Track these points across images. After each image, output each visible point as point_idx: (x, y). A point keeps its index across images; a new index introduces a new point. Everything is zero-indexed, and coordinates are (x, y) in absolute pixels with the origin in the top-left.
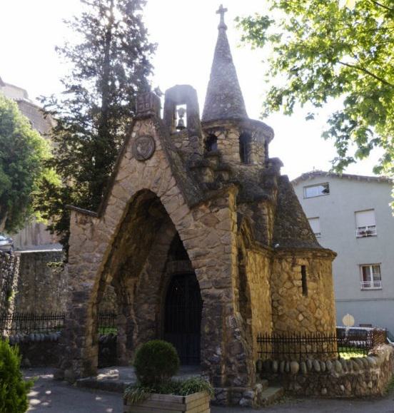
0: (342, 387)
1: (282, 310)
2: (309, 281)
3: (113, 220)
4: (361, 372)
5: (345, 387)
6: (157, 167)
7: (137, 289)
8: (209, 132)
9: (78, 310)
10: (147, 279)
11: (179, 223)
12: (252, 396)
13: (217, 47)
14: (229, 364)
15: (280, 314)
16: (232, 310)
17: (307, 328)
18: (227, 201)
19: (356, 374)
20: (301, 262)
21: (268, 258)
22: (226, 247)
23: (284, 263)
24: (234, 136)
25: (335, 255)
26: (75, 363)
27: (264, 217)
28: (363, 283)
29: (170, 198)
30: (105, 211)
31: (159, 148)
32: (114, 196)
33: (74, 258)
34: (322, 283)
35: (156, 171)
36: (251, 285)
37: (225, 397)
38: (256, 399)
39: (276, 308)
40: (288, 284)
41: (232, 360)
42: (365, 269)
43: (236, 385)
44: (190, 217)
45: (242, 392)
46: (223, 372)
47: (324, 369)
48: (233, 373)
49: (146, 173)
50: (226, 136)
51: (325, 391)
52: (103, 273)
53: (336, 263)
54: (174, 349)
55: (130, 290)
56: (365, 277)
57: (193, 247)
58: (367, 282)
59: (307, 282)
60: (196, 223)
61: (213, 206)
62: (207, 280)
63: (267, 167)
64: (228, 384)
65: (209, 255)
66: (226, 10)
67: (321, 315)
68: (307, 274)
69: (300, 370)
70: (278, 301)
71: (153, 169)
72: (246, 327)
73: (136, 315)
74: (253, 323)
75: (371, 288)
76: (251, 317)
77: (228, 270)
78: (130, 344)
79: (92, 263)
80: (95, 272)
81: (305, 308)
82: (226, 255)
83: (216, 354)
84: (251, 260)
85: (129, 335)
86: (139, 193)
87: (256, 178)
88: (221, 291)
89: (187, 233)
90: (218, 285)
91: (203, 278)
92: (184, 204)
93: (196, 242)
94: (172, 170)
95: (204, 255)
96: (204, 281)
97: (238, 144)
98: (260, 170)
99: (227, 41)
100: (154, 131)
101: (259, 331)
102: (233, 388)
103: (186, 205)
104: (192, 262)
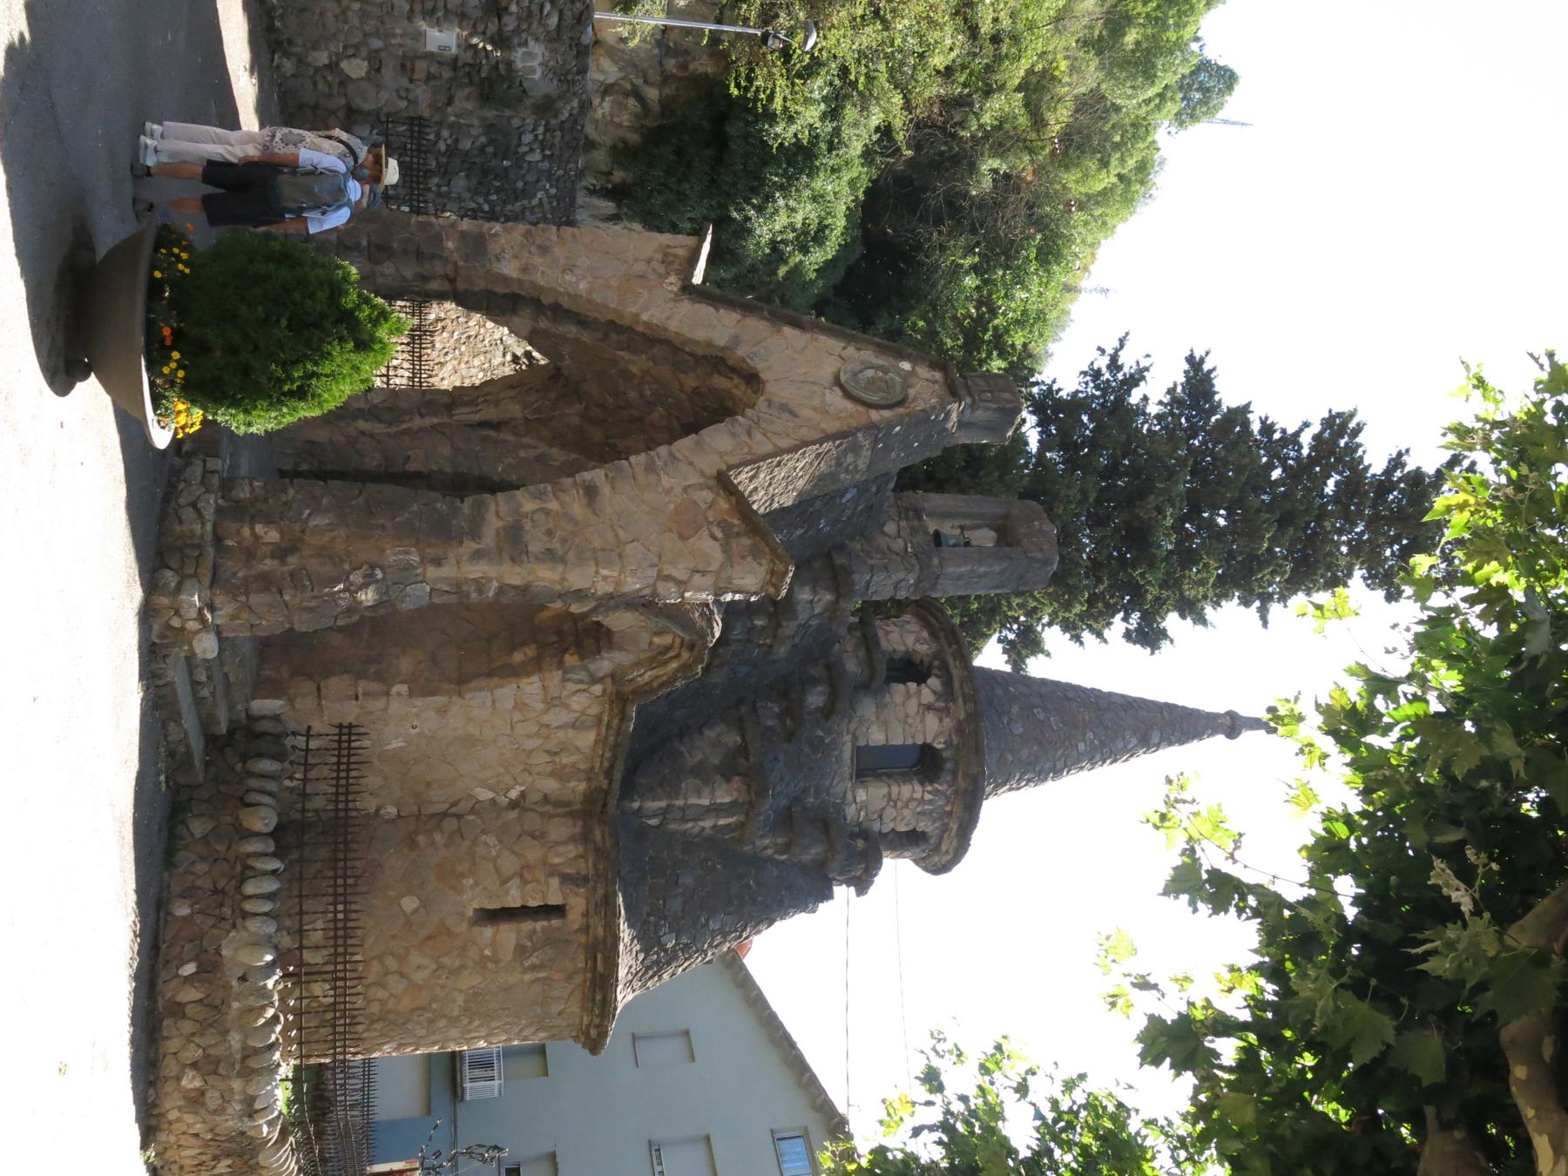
0: (189, 969)
1: (433, 844)
4: (235, 1040)
5: (188, 979)
6: (823, 410)
7: (492, 433)
10: (522, 454)
15: (421, 839)
20: (577, 905)
23: (572, 850)
24: (932, 730)
31: (875, 415)
34: (514, 978)
35: (814, 409)
39: (438, 827)
40: (509, 864)
47: (249, 906)
50: (929, 707)
60: (678, 490)
63: (853, 836)
68: (540, 925)
70: (459, 831)
71: (816, 402)
73: (421, 429)
76: (411, 694)
77: (550, 556)
84: (579, 702)
87: (817, 793)
98: (840, 809)
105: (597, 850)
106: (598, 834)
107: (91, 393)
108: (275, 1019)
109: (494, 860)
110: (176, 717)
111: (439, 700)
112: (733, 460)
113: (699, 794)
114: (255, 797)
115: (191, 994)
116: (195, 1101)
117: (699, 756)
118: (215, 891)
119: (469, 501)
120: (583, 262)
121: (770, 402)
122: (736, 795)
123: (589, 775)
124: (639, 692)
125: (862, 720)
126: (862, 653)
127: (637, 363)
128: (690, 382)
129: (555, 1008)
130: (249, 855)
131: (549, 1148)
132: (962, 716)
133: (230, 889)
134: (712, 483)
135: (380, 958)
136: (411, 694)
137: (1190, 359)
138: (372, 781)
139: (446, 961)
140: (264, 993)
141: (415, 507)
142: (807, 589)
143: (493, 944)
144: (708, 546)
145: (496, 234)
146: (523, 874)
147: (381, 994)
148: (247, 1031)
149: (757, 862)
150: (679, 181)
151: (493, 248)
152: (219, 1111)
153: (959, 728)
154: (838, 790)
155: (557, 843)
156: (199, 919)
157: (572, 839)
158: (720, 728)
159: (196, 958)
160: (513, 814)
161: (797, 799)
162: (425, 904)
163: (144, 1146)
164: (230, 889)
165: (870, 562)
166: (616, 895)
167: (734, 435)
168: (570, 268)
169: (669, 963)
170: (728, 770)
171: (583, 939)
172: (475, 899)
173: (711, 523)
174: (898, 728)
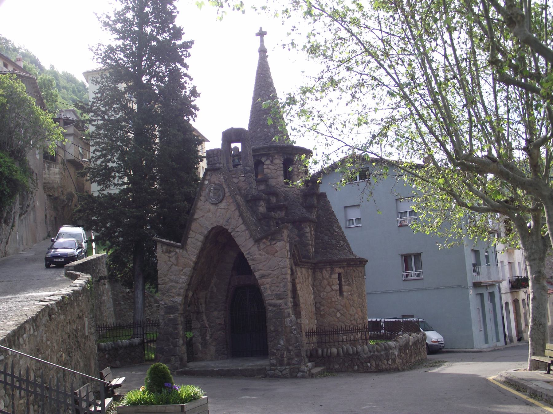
0: (369, 364)
1: (323, 310)
2: (344, 285)
3: (193, 250)
4: (383, 353)
8: (257, 158)
9: (171, 320)
11: (247, 252)
12: (306, 371)
13: (258, 71)
14: (289, 351)
16: (289, 314)
17: (343, 322)
18: (282, 236)
19: (379, 354)
20: (338, 270)
21: (311, 269)
22: (283, 270)
24: (279, 161)
25: (367, 261)
26: (173, 358)
27: (307, 234)
28: (404, 273)
29: (239, 233)
30: (186, 243)
31: (228, 194)
32: (193, 231)
33: (163, 280)
34: (355, 286)
35: (227, 212)
36: (300, 293)
37: (288, 372)
38: (308, 372)
39: (319, 308)
40: (328, 288)
41: (291, 348)
42: (406, 258)
43: (294, 364)
44: (255, 248)
45: (298, 369)
46: (285, 356)
48: (291, 357)
49: (218, 214)
50: (272, 162)
51: (356, 367)
52: (187, 290)
53: (367, 266)
56: (407, 267)
57: (259, 270)
58: (410, 272)
60: (260, 252)
61: (272, 240)
62: (270, 293)
64: (289, 364)
65: (271, 276)
66: (265, 33)
67: (355, 312)
69: (338, 353)
70: (320, 303)
72: (299, 325)
73: (208, 321)
74: (303, 322)
75: (413, 278)
78: (205, 344)
79: (178, 283)
80: (182, 291)
81: (342, 307)
82: (283, 276)
83: (280, 345)
84: (299, 273)
85: (203, 336)
86: (213, 229)
87: (298, 198)
88: (281, 301)
89: (253, 260)
90: (279, 297)
92: (250, 238)
93: (260, 266)
94: (239, 212)
95: (268, 276)
96: (269, 294)
97: (282, 169)
98: (302, 191)
99: (271, 84)
100: (223, 180)
101: (307, 327)
102: (292, 366)
103: (251, 239)
104: (259, 281)
109: (327, 293)
130: (343, 353)
135: (351, 321)
147: (359, 320)
149: (318, 217)
159: (366, 363)
161: (302, 205)
171: (346, 268)
173: (271, 244)
174: (278, 173)
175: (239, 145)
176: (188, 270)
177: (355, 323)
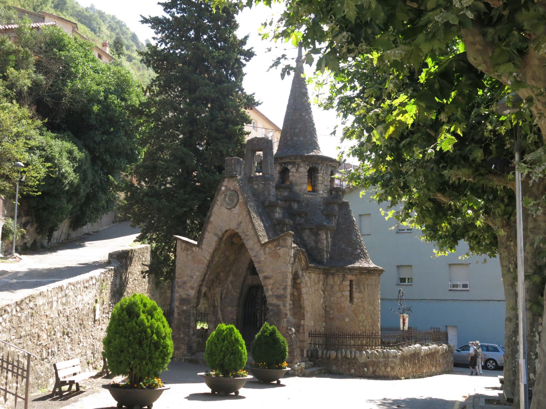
0: (366, 369)
1: (333, 314)
4: (381, 360)
5: (368, 370)
7: (223, 296)
9: (183, 311)
10: (230, 288)
15: (331, 316)
20: (350, 277)
23: (336, 278)
24: (304, 170)
27: (322, 241)
31: (241, 201)
35: (239, 217)
40: (339, 294)
44: (262, 252)
47: (353, 357)
50: (297, 170)
52: (201, 286)
54: (171, 350)
55: (218, 297)
59: (354, 293)
60: (266, 256)
61: (278, 245)
63: (331, 194)
68: (354, 287)
69: (337, 356)
71: (237, 216)
75: (459, 289)
76: (304, 319)
77: (285, 289)
84: (307, 278)
86: (226, 231)
90: (279, 297)
91: (269, 293)
98: (324, 199)
105: (336, 272)
106: (333, 271)
107: (242, 391)
108: (377, 351)
109: (338, 298)
110: (314, 371)
111: (305, 313)
112: (256, 241)
113: (323, 243)
114: (328, 356)
115: (371, 369)
116: (393, 368)
117: (312, 242)
118: (349, 364)
119: (269, 307)
120: (188, 272)
121: (237, 229)
122: (324, 233)
123: (319, 274)
124: (307, 264)
125: (300, 191)
126: (281, 190)
127: (216, 259)
128: (223, 245)
129: (374, 283)
131: (396, 268)
132: (300, 160)
133: (349, 361)
134: (263, 247)
136: (304, 319)
137: (143, 22)
138: (318, 329)
139: (361, 311)
140: (372, 353)
141: (272, 319)
142: (276, 214)
143: (358, 299)
144: (282, 251)
145: (180, 295)
146: (342, 291)
147: (368, 326)
148: (380, 357)
149: (338, 224)
150: (55, 209)
151: (184, 296)
152: (395, 363)
153: (304, 162)
154: (319, 199)
155: (334, 282)
156: (355, 367)
157: (333, 278)
158: (304, 235)
159: (363, 368)
160: (326, 293)
162: (347, 316)
163: (401, 379)
164: (349, 361)
165: (267, 195)
166: (349, 268)
167: (248, 239)
168: (192, 277)
169: (363, 251)
170: (317, 235)
171: (358, 276)
172: (348, 303)
175: (261, 153)
176: (203, 267)
177: (364, 329)
